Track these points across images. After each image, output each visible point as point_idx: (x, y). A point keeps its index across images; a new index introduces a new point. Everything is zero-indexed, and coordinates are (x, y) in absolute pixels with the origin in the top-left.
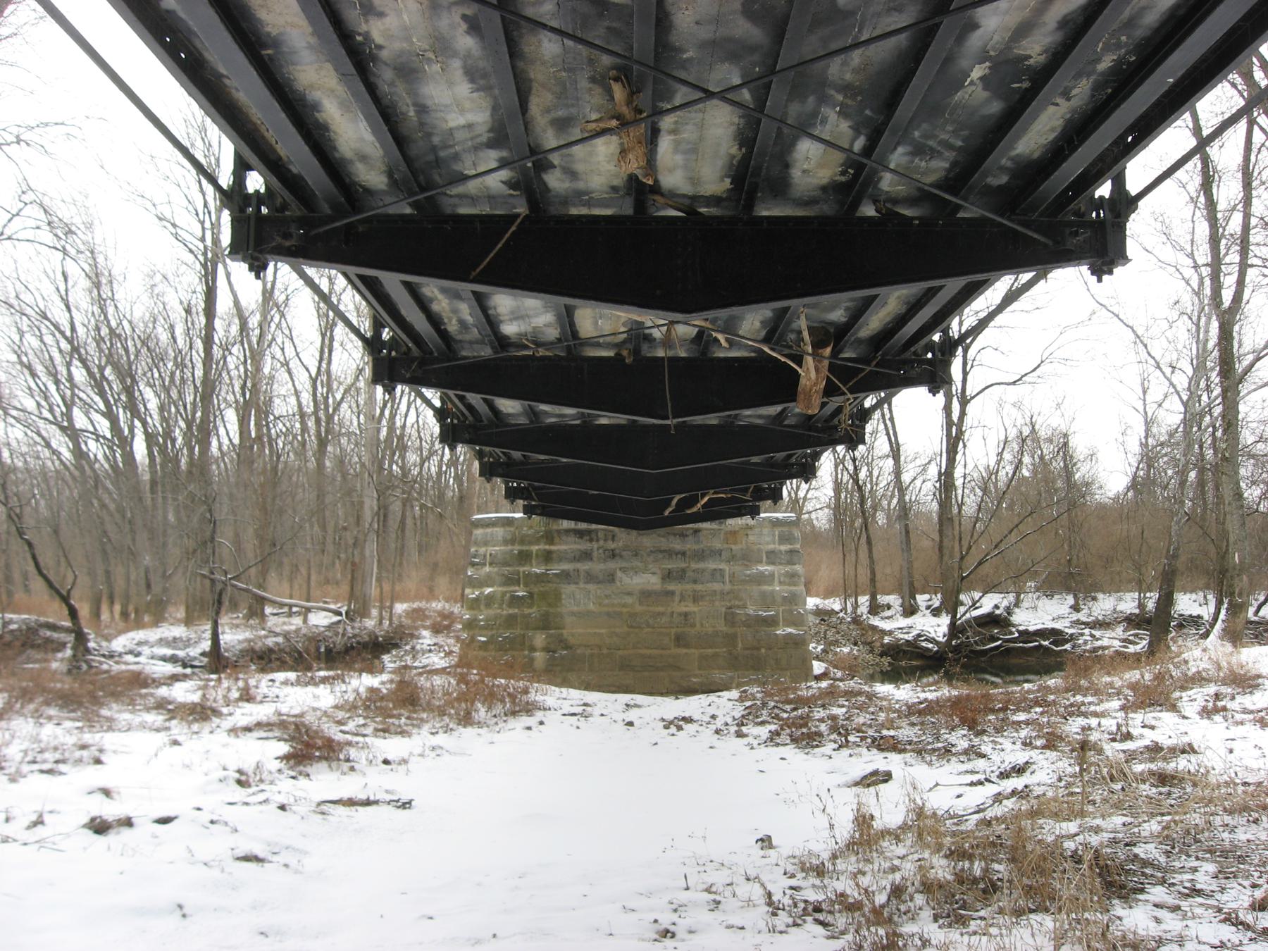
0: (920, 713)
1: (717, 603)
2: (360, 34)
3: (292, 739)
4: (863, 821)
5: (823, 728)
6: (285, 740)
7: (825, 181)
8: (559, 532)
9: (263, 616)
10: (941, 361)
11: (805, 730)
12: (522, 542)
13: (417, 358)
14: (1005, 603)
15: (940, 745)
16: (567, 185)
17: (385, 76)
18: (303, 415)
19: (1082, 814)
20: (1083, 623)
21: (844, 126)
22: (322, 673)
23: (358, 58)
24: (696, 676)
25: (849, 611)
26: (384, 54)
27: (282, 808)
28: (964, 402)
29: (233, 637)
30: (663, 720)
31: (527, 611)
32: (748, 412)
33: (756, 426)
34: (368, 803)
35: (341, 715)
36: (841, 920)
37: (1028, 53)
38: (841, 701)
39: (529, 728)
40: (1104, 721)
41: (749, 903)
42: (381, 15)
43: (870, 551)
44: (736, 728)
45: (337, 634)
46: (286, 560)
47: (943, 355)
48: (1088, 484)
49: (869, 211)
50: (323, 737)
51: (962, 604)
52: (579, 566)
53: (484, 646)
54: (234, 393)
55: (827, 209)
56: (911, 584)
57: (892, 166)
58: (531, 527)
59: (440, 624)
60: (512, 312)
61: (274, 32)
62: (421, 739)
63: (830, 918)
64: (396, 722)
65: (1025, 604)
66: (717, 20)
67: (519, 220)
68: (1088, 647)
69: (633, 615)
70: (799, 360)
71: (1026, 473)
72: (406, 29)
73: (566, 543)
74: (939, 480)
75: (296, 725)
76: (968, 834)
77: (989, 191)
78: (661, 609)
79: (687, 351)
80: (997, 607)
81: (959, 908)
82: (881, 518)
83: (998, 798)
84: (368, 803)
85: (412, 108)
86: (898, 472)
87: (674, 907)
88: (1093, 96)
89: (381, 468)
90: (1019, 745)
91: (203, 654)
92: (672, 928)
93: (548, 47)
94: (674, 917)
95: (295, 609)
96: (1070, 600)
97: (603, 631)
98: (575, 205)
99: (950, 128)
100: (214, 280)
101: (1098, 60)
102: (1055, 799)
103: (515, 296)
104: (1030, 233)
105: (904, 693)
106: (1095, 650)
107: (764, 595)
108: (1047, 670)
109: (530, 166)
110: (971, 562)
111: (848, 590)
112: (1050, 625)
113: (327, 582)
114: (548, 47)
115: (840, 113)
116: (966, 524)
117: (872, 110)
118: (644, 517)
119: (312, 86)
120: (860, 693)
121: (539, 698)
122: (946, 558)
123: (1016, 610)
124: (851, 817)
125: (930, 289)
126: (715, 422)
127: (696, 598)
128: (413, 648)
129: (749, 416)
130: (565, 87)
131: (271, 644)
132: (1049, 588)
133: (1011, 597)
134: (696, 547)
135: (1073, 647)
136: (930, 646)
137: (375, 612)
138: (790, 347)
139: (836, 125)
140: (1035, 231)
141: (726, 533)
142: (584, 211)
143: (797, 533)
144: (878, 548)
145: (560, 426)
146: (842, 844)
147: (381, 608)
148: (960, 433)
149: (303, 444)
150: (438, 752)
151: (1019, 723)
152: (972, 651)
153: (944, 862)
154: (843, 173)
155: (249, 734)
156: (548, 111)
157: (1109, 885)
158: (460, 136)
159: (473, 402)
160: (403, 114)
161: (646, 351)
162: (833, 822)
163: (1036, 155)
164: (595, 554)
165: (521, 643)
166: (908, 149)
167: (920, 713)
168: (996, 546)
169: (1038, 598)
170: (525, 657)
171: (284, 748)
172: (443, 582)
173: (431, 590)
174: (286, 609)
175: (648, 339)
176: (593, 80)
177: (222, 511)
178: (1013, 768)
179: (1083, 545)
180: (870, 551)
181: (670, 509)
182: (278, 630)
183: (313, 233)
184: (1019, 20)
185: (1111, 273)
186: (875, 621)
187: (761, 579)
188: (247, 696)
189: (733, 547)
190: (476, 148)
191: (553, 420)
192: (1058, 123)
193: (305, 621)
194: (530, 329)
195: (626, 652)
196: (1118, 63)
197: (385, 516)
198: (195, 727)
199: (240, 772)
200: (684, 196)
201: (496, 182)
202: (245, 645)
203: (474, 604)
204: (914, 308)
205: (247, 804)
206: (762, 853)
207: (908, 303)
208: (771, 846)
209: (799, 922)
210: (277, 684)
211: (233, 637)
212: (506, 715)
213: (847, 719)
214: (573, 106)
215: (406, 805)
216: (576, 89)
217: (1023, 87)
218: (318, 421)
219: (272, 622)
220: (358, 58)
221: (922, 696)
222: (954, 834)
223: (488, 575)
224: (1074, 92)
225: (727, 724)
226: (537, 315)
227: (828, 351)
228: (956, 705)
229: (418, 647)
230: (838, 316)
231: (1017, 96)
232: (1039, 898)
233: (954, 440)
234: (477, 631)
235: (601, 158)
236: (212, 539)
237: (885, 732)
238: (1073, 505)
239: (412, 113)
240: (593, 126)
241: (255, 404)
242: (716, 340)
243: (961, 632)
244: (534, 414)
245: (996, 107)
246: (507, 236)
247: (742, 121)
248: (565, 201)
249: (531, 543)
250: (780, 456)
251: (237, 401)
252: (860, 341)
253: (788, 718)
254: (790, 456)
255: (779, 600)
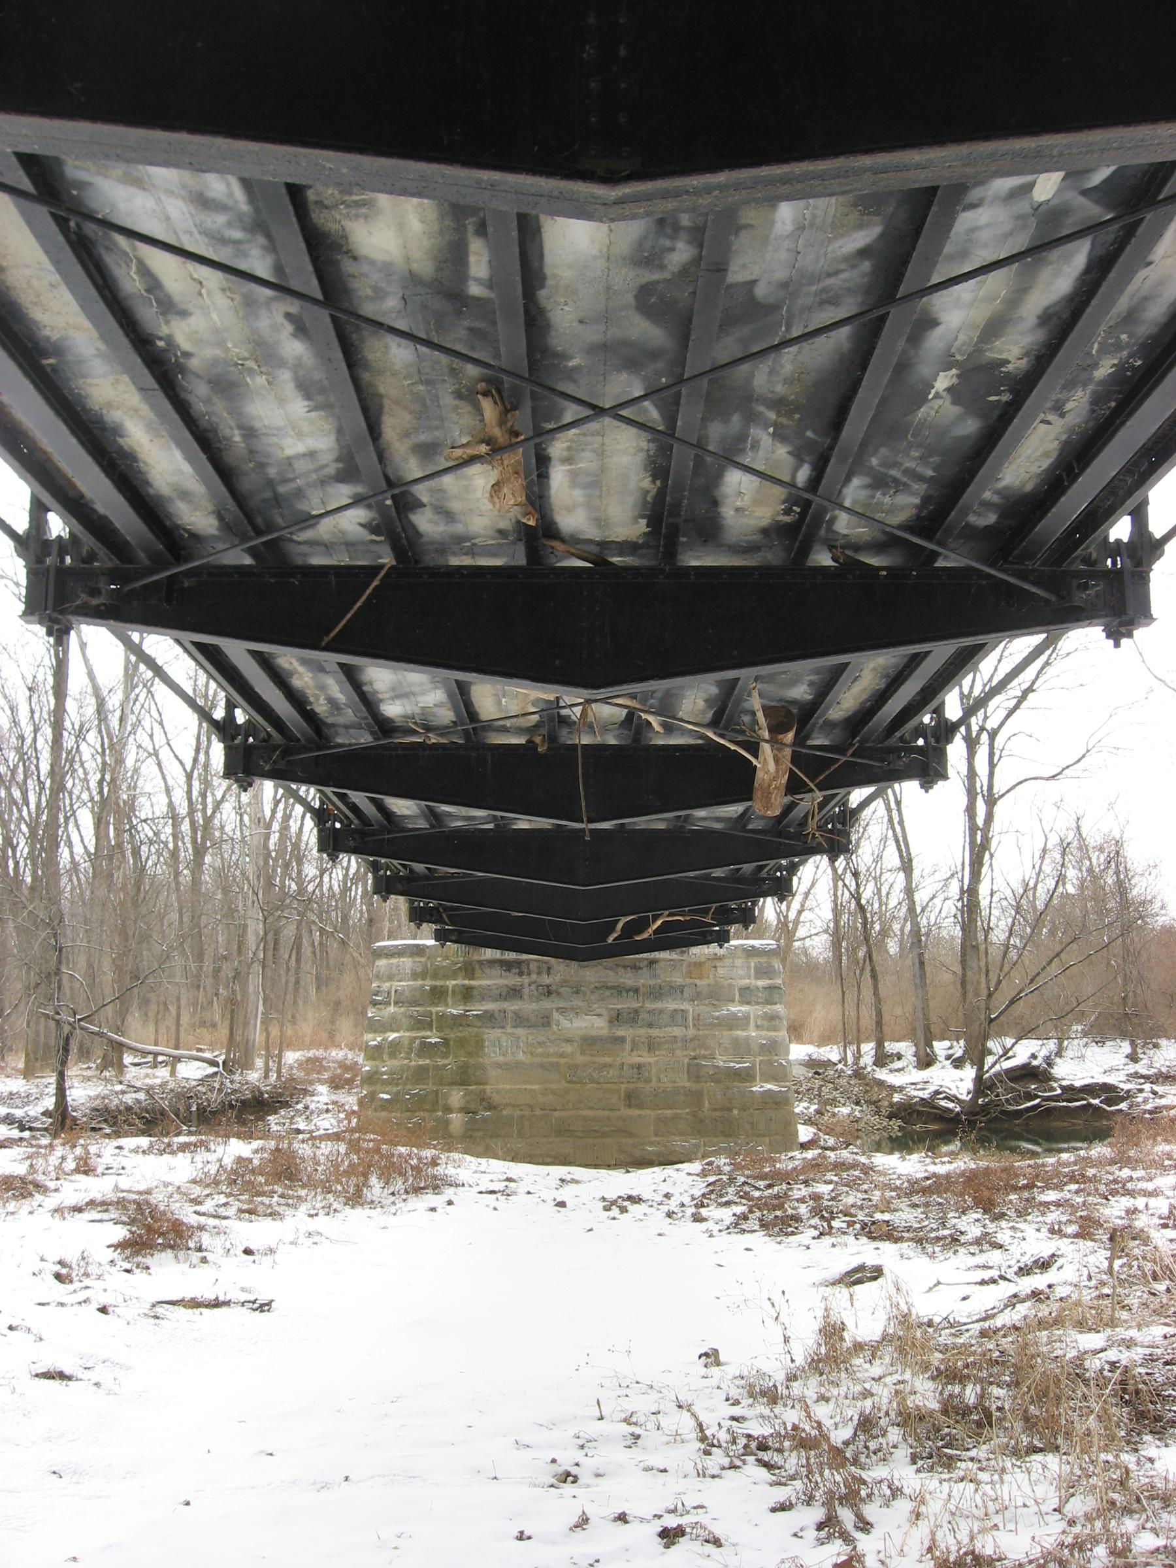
0: (925, 1191)
1: (678, 1052)
2: (161, 339)
3: (132, 1222)
4: (832, 1331)
5: (803, 1210)
6: (124, 1223)
7: (765, 522)
8: (480, 963)
9: (121, 1067)
10: (935, 749)
11: (778, 1213)
12: (435, 976)
13: (280, 746)
14: (1044, 1052)
15: (946, 1232)
16: (441, 528)
17: (198, 392)
18: (175, 819)
19: (1112, 1323)
20: (1142, 1077)
21: (782, 452)
22: (182, 1139)
23: (162, 370)
24: (651, 1144)
25: (850, 1060)
26: (194, 363)
27: (103, 1310)
28: (991, 802)
29: (83, 1092)
30: (604, 1199)
31: (441, 1062)
32: (701, 813)
33: (712, 832)
34: (216, 1304)
35: (197, 1191)
36: (792, 1461)
37: (1004, 356)
38: (830, 1176)
39: (433, 1209)
40: (1153, 1202)
41: (677, 1438)
42: (184, 314)
43: (876, 987)
44: (693, 1210)
45: (212, 1090)
46: (153, 996)
47: (937, 741)
48: (1143, 903)
49: (823, 559)
50: (168, 1221)
51: (990, 1053)
52: (506, 1005)
53: (385, 1106)
54: (88, 789)
55: (773, 556)
56: (927, 1028)
57: (847, 504)
58: (447, 958)
59: (340, 1076)
60: (393, 689)
61: (55, 336)
62: (296, 1221)
63: (777, 1459)
64: (266, 1200)
65: (1069, 1053)
66: (606, 317)
67: (383, 573)
68: (1149, 1107)
69: (573, 1067)
70: (754, 749)
71: (1071, 890)
72: (216, 331)
73: (490, 978)
74: (961, 899)
75: (138, 1204)
76: (964, 1349)
77: (973, 533)
78: (608, 1060)
79: (617, 737)
80: (1034, 1056)
81: (943, 1447)
82: (893, 947)
83: (1015, 1300)
84: (216, 1304)
85: (237, 432)
86: (909, 891)
87: (581, 1442)
88: (1093, 411)
89: (270, 884)
90: (1044, 1232)
91: (46, 1113)
92: (574, 1470)
93: (396, 356)
94: (579, 1456)
95: (160, 1058)
96: (1126, 1048)
97: (536, 1087)
98: (455, 554)
99: (915, 454)
100: (66, 652)
101: (1095, 366)
102: (1078, 1303)
103: (392, 668)
104: (1026, 586)
105: (910, 1166)
106: (1156, 1111)
107: (736, 1042)
108: (1099, 1135)
109: (395, 505)
110: (1001, 1001)
111: (848, 1035)
112: (1101, 1079)
113: (203, 1024)
114: (399, 354)
115: (774, 435)
116: (995, 953)
117: (814, 431)
118: (585, 945)
119: (109, 405)
120: (854, 1166)
121: (451, 1171)
122: (970, 995)
123: (1058, 1060)
124: (817, 1325)
125: (916, 655)
126: (661, 826)
127: (652, 1046)
128: (306, 1108)
129: (704, 819)
130: (424, 404)
131: (130, 1102)
132: (1100, 1033)
133: (1052, 1045)
134: (652, 982)
135: (1130, 1107)
136: (951, 1105)
137: (259, 1063)
138: (742, 732)
139: (771, 451)
140: (1034, 583)
141: (689, 965)
142: (467, 561)
143: (777, 964)
144: (886, 985)
145: (467, 831)
146: (800, 1360)
147: (268, 1057)
148: (986, 840)
149: (174, 854)
150: (316, 1239)
151: (1046, 1204)
152: (1003, 1112)
153: (930, 1385)
154: (787, 512)
155: (78, 1215)
156: (406, 434)
157: (1140, 1416)
158: (301, 466)
159: (356, 801)
160: (228, 439)
161: (567, 738)
162: (788, 1333)
163: (1029, 488)
164: (526, 991)
165: (433, 1102)
166: (866, 480)
167: (925, 1191)
168: (1032, 981)
169: (1086, 1045)
170: (436, 1120)
171: (120, 1233)
172: (345, 1026)
173: (331, 1035)
174: (150, 1058)
175: (564, 721)
176: (458, 395)
177: (75, 938)
178: (1035, 1262)
179: (1141, 979)
180: (876, 987)
181: (615, 935)
182: (138, 1084)
183: (127, 588)
184: (988, 314)
185: (1130, 635)
186: (882, 1074)
187: (733, 1022)
188: (85, 1168)
189: (698, 982)
190: (323, 482)
191: (459, 823)
192: (1053, 446)
193: (173, 1073)
194: (417, 711)
195: (564, 1114)
196: (1121, 368)
197: (276, 943)
198: (12, 1206)
199: (61, 1263)
200: (590, 541)
201: (353, 521)
202: (98, 1101)
203: (375, 1053)
204: (896, 681)
205: (62, 1305)
206: (703, 1371)
207: (887, 676)
208: (718, 1363)
209: (738, 1463)
210: (125, 1152)
211: (83, 1092)
212: (407, 1192)
213: (833, 1199)
214: (437, 428)
215: (264, 1307)
216: (439, 406)
217: (1003, 402)
218: (193, 823)
219: (131, 1073)
220: (162, 370)
221: (932, 1169)
222: (944, 1350)
223: (393, 1017)
224: (1069, 406)
225: (683, 1205)
226: (423, 693)
227: (790, 736)
228: (971, 1180)
229: (313, 1106)
230: (801, 692)
231: (997, 412)
232: (1043, 1432)
233: (979, 851)
234: (378, 1087)
235: (479, 494)
236: (58, 972)
237: (878, 1216)
238: (1127, 928)
239: (237, 438)
240: (458, 452)
241: (114, 808)
242: (649, 723)
243: (989, 1088)
244: (433, 815)
245: (971, 427)
246: (368, 592)
247: (652, 446)
248: (443, 549)
249: (446, 977)
250: (748, 868)
251: (92, 799)
252: (830, 725)
253: (760, 1198)
254: (761, 868)
255: (756, 1048)
